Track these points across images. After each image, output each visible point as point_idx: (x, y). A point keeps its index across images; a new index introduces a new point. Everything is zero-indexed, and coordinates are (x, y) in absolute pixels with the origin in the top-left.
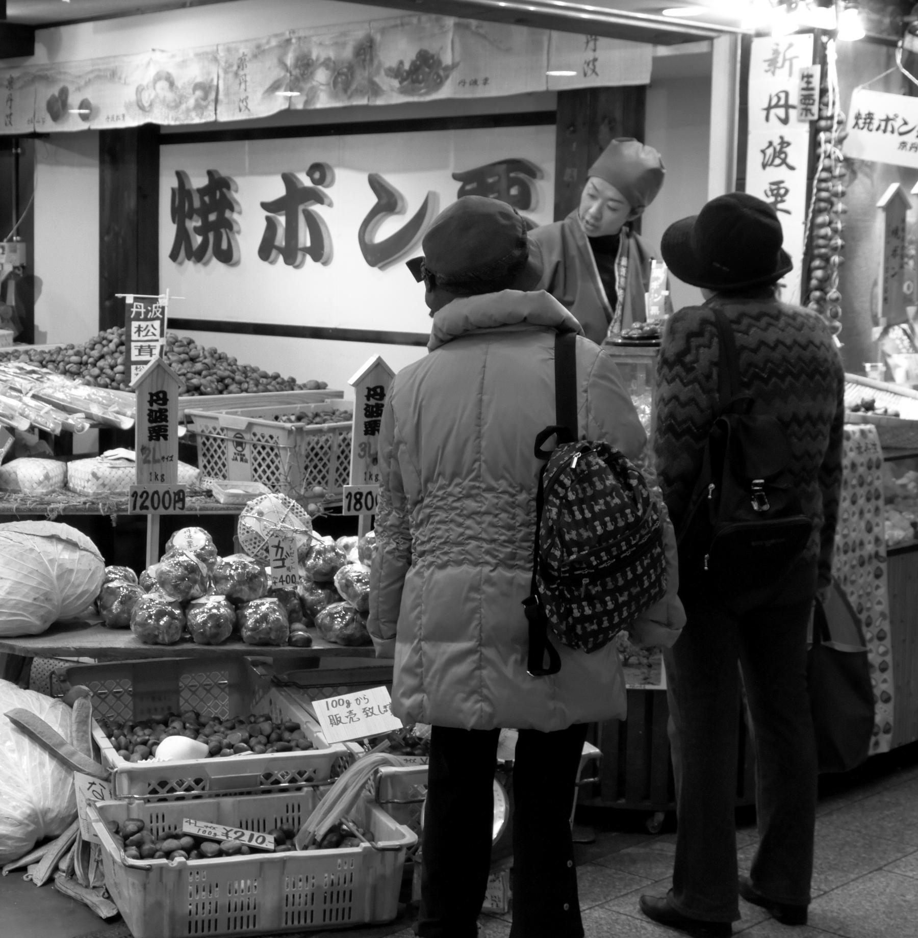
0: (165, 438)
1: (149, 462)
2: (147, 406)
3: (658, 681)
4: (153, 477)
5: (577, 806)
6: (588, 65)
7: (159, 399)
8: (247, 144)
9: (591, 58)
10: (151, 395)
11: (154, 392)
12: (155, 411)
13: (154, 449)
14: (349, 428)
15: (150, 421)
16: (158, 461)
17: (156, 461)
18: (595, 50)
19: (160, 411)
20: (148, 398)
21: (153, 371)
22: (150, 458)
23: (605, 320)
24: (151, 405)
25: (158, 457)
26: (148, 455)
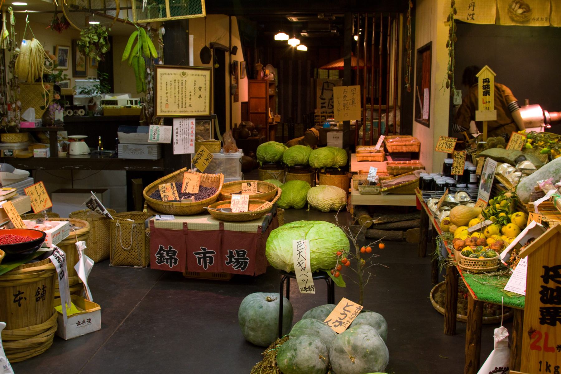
0: (489, 95)
1: (539, 348)
2: (540, 282)
3: (97, 150)
4: (544, 367)
5: (187, 20)
6: (470, 15)
7: (486, 81)
8: (233, 115)
9: (472, 13)
10: (546, 268)
11: (551, 265)
12: (551, 289)
13: (547, 335)
14: (164, 15)
15: (542, 300)
16: (552, 350)
17: (547, 349)
18: (473, 10)
19: (487, 85)
20: (542, 272)
21: (550, 240)
22: (541, 343)
23: (275, 194)
24: (546, 281)
25: (551, 344)
26: (539, 340)
